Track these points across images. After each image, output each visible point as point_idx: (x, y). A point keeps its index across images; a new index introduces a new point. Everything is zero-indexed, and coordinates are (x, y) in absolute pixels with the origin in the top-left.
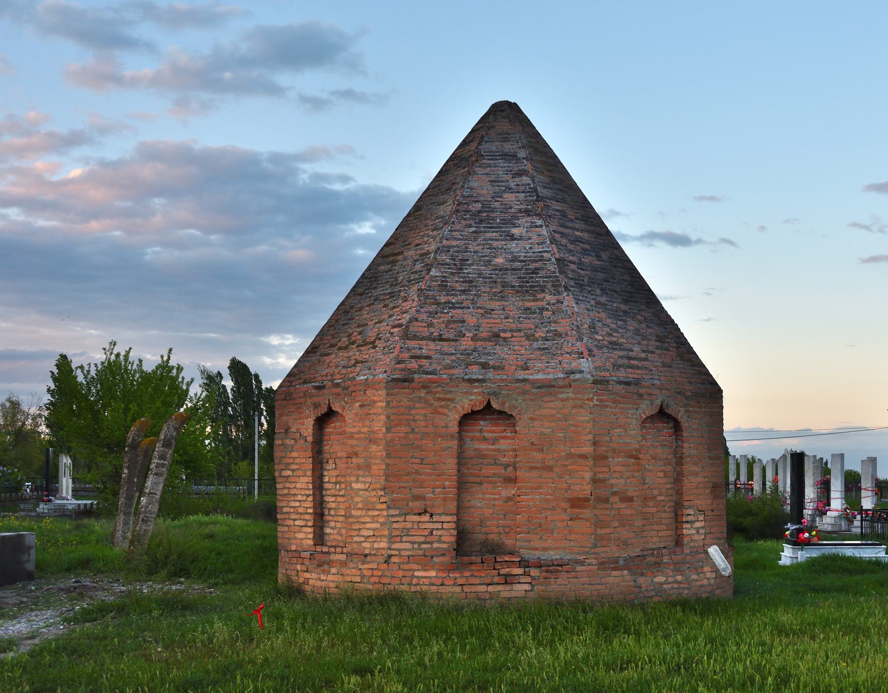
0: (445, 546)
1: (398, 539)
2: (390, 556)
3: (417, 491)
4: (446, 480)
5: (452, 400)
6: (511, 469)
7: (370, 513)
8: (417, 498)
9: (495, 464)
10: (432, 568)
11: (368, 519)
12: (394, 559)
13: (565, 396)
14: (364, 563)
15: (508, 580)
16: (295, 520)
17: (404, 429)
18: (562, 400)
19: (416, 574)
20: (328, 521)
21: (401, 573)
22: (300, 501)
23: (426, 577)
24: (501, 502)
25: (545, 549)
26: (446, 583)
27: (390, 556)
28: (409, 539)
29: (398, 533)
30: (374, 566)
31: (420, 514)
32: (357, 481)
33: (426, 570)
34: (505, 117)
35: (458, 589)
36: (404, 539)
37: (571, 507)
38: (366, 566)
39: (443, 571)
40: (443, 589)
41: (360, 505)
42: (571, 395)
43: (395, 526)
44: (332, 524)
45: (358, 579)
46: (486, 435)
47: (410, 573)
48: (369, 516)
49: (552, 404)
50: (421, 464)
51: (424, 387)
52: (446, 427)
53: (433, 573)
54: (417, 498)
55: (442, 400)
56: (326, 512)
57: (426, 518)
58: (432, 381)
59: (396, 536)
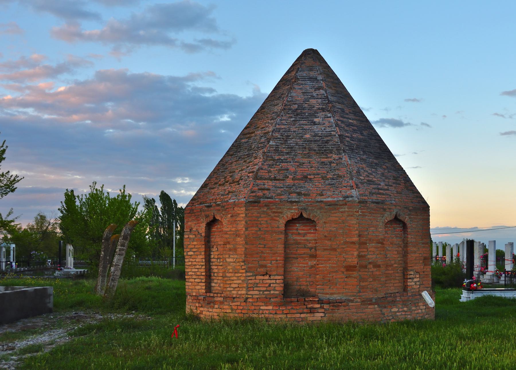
1: (252, 289)
4: (278, 256)
5: (281, 213)
7: (237, 275)
8: (262, 266)
9: (305, 247)
10: (270, 304)
11: (235, 278)
13: (343, 210)
14: (233, 302)
15: (312, 311)
16: (195, 279)
17: (257, 229)
18: (342, 212)
19: (261, 308)
20: (213, 280)
21: (253, 308)
23: (267, 310)
24: (308, 268)
25: (332, 294)
27: (247, 298)
28: (258, 289)
29: (252, 286)
30: (239, 304)
31: (264, 275)
32: (229, 257)
33: (266, 306)
34: (311, 57)
36: (255, 289)
37: (346, 271)
39: (276, 306)
41: (231, 271)
42: (347, 209)
43: (250, 281)
45: (230, 311)
46: (300, 232)
48: (236, 277)
49: (336, 215)
50: (264, 247)
51: (266, 206)
52: (278, 227)
53: (270, 308)
54: (262, 266)
57: (267, 277)
58: (270, 202)
59: (250, 287)
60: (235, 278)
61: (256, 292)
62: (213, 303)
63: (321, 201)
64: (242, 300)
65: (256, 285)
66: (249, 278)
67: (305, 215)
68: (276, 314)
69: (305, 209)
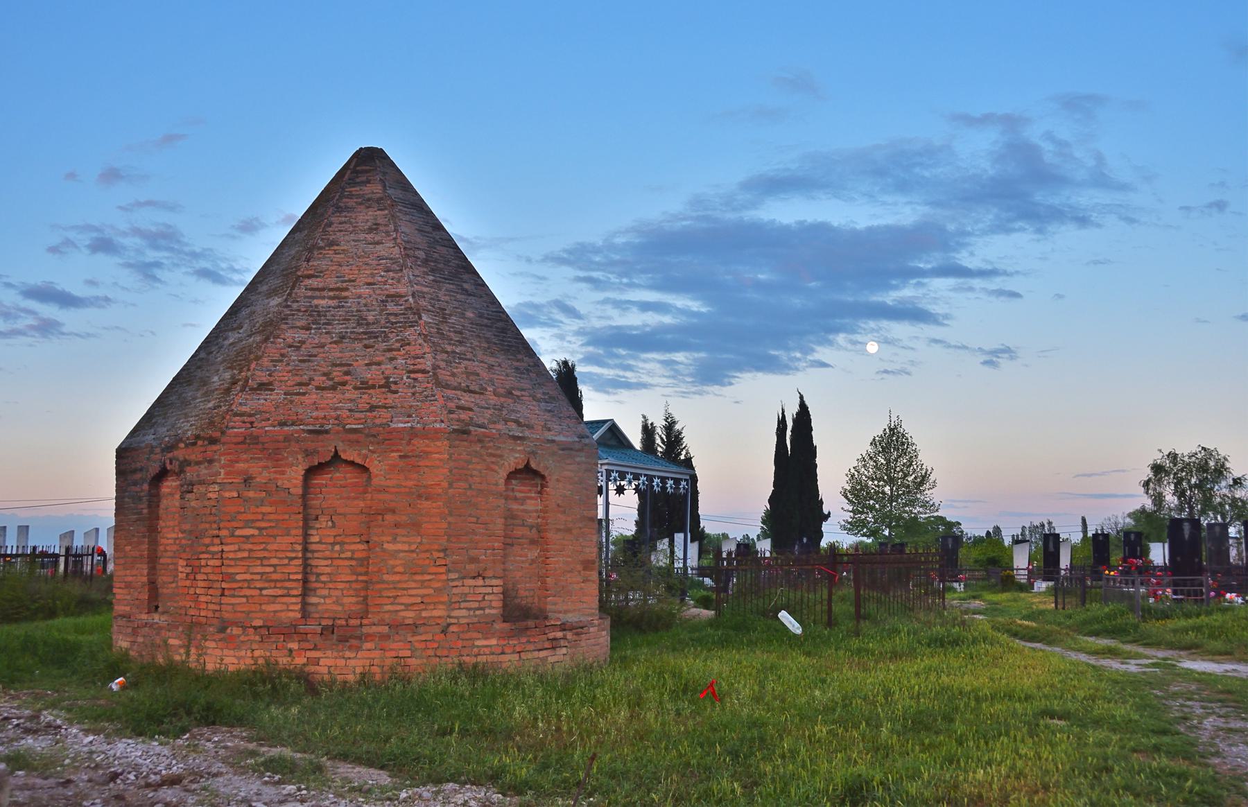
0: (493, 611)
2: (449, 625)
3: (473, 553)
5: (501, 456)
6: (534, 530)
7: (418, 578)
8: (474, 560)
9: (523, 525)
10: (493, 635)
11: (413, 585)
12: (453, 629)
14: (414, 634)
15: (554, 645)
16: (261, 589)
19: (478, 643)
20: (315, 590)
21: (460, 643)
22: (274, 566)
23: (486, 646)
25: (566, 612)
26: (507, 651)
27: (449, 625)
28: (467, 605)
29: (457, 599)
30: (429, 637)
31: (474, 578)
32: (394, 541)
33: (486, 639)
34: (369, 162)
35: (516, 656)
36: (463, 605)
38: (419, 638)
39: (503, 638)
40: (502, 658)
41: (400, 569)
43: (455, 591)
44: (319, 592)
45: (408, 653)
47: (470, 643)
48: (415, 581)
49: (570, 467)
51: (480, 441)
52: (497, 484)
53: (494, 642)
54: (474, 560)
55: (494, 456)
56: (313, 578)
57: (480, 582)
58: (485, 435)
60: (413, 585)
61: (464, 613)
62: (359, 638)
63: (553, 441)
64: (437, 629)
65: (464, 598)
66: (452, 584)
67: (533, 465)
68: (503, 653)
69: (534, 453)
